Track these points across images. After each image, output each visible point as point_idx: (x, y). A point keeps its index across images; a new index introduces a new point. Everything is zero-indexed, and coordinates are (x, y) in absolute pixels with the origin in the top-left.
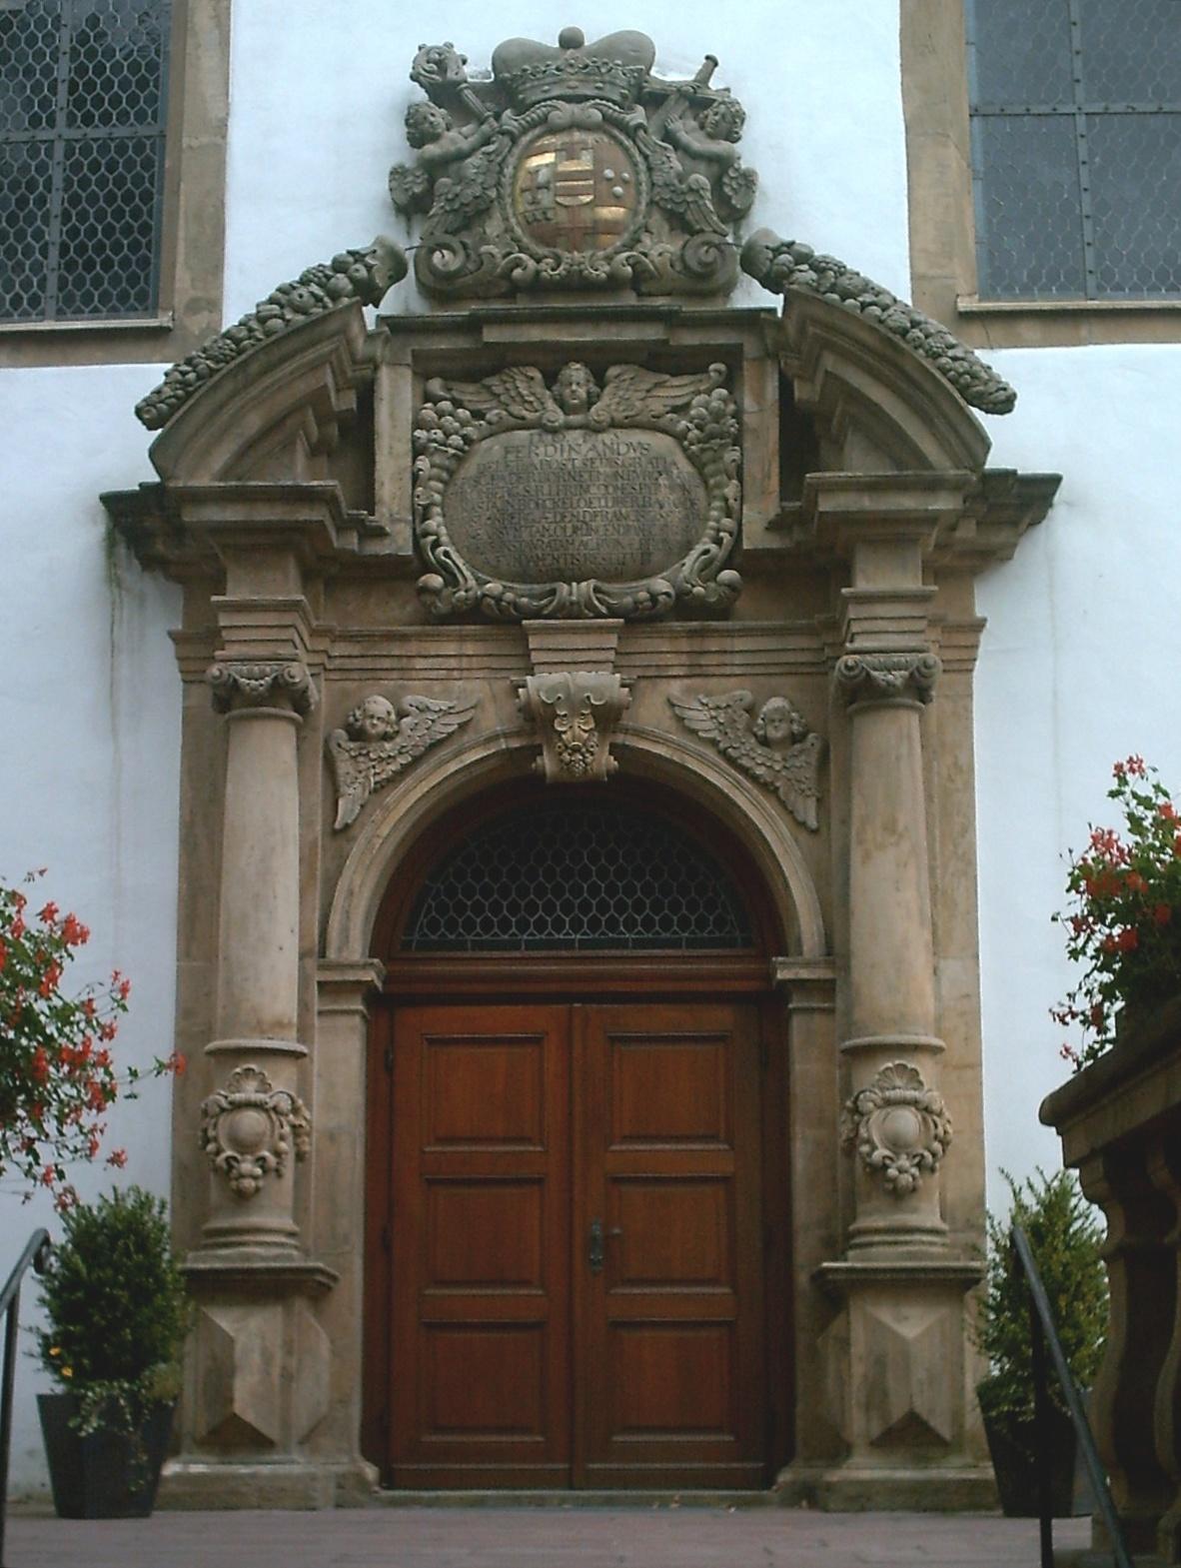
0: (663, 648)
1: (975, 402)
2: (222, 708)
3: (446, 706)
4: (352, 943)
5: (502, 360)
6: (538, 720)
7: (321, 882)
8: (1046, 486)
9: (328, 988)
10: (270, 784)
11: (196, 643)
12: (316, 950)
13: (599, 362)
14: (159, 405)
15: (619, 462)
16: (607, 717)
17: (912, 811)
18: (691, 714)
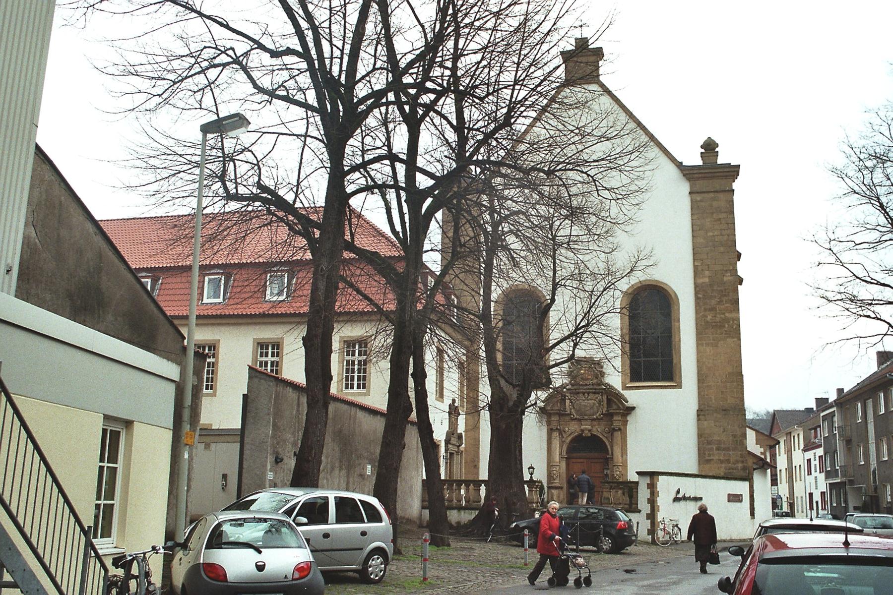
0: (595, 423)
1: (172, 497)
2: (550, 431)
3: (573, 428)
4: (564, 453)
5: (578, 393)
6: (582, 431)
7: (561, 447)
8: (633, 408)
9: (561, 457)
10: (556, 444)
11: (549, 423)
12: (561, 454)
13: (588, 393)
14: (432, 96)
15: (589, 403)
16: (589, 431)
17: (620, 442)
18: (598, 430)
